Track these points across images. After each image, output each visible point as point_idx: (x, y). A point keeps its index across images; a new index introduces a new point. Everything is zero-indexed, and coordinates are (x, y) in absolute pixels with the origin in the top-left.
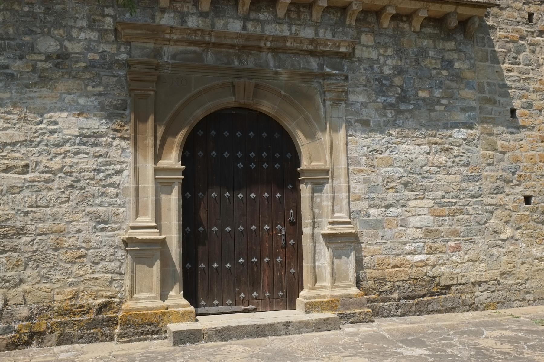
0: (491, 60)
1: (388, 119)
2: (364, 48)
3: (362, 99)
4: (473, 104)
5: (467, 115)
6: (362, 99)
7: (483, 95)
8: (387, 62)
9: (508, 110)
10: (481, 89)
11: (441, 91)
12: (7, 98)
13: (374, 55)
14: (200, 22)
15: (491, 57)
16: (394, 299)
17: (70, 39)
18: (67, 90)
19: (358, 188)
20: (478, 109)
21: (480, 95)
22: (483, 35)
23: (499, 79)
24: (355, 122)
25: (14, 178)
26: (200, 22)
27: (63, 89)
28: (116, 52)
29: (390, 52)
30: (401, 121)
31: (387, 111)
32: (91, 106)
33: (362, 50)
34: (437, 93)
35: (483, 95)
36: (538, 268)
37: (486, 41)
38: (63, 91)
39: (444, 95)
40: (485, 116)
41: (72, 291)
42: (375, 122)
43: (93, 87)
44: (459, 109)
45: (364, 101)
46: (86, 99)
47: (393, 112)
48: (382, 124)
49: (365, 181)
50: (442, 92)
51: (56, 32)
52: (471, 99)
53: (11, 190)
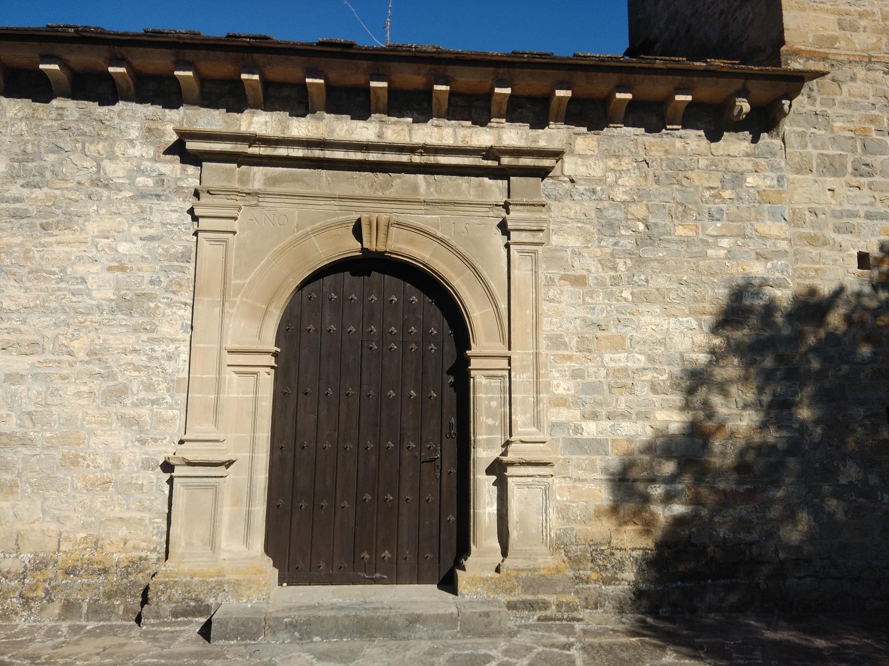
0: (818, 171)
1: (620, 273)
2: (580, 161)
3: (573, 242)
4: (783, 245)
5: (769, 265)
6: (573, 242)
7: (802, 230)
8: (620, 182)
9: (851, 256)
10: (795, 220)
11: (719, 225)
12: (17, 245)
13: (596, 169)
14: (310, 128)
15: (818, 165)
16: (626, 580)
17: (112, 157)
18: (102, 232)
19: (563, 386)
20: (791, 255)
21: (796, 230)
22: (803, 129)
23: (833, 202)
24: (561, 279)
25: (21, 364)
26: (310, 128)
27: (96, 230)
28: (179, 176)
29: (626, 163)
30: (643, 277)
31: (617, 260)
32: (137, 255)
33: (576, 164)
34: (713, 228)
35: (802, 230)
36: (13, 338)
37: (808, 139)
38: (96, 234)
39: (724, 232)
40: (805, 266)
41: (85, 538)
42: (596, 278)
43: (141, 227)
44: (754, 255)
45: (578, 244)
46: (130, 245)
47: (629, 261)
48: (608, 282)
49: (576, 374)
50: (722, 227)
51: (92, 148)
52: (778, 238)
53: (13, 378)
